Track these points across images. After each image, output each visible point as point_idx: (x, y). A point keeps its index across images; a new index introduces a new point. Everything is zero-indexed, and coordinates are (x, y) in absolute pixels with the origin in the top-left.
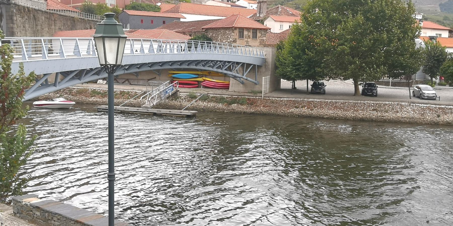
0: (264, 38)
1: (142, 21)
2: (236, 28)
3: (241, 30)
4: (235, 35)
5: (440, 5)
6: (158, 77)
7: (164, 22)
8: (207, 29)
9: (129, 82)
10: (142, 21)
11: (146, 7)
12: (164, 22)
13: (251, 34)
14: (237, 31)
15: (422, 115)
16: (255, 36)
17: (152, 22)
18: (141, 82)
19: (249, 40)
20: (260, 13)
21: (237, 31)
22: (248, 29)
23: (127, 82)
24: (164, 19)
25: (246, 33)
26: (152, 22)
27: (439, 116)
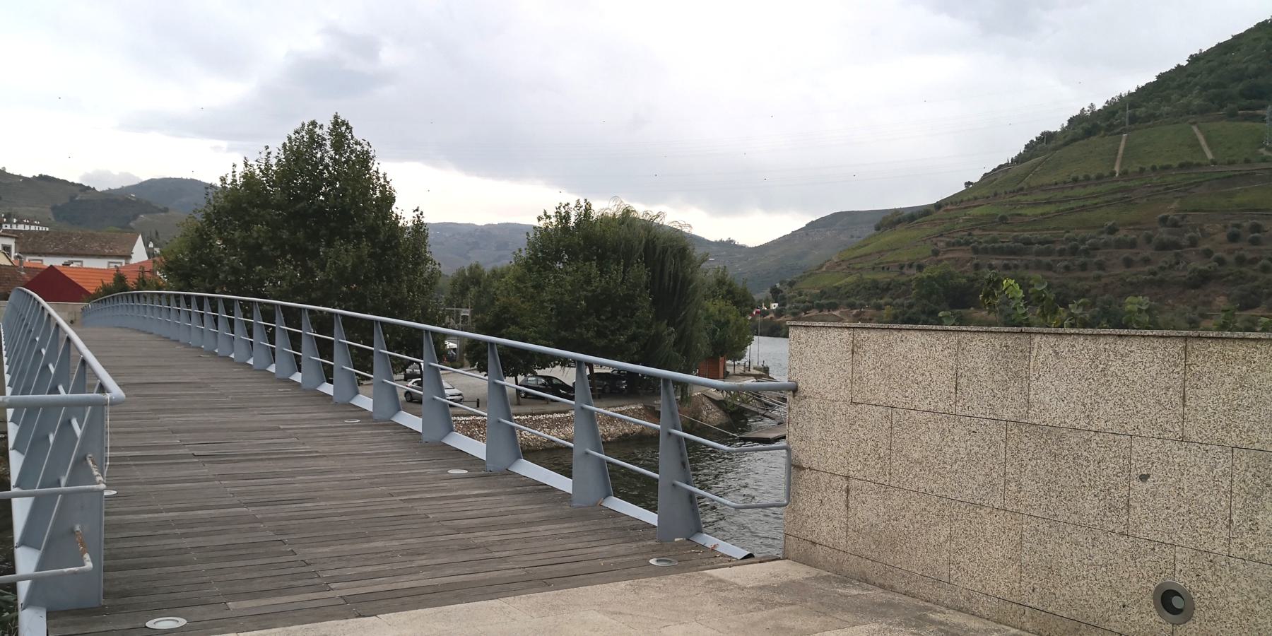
5: (54, 208)
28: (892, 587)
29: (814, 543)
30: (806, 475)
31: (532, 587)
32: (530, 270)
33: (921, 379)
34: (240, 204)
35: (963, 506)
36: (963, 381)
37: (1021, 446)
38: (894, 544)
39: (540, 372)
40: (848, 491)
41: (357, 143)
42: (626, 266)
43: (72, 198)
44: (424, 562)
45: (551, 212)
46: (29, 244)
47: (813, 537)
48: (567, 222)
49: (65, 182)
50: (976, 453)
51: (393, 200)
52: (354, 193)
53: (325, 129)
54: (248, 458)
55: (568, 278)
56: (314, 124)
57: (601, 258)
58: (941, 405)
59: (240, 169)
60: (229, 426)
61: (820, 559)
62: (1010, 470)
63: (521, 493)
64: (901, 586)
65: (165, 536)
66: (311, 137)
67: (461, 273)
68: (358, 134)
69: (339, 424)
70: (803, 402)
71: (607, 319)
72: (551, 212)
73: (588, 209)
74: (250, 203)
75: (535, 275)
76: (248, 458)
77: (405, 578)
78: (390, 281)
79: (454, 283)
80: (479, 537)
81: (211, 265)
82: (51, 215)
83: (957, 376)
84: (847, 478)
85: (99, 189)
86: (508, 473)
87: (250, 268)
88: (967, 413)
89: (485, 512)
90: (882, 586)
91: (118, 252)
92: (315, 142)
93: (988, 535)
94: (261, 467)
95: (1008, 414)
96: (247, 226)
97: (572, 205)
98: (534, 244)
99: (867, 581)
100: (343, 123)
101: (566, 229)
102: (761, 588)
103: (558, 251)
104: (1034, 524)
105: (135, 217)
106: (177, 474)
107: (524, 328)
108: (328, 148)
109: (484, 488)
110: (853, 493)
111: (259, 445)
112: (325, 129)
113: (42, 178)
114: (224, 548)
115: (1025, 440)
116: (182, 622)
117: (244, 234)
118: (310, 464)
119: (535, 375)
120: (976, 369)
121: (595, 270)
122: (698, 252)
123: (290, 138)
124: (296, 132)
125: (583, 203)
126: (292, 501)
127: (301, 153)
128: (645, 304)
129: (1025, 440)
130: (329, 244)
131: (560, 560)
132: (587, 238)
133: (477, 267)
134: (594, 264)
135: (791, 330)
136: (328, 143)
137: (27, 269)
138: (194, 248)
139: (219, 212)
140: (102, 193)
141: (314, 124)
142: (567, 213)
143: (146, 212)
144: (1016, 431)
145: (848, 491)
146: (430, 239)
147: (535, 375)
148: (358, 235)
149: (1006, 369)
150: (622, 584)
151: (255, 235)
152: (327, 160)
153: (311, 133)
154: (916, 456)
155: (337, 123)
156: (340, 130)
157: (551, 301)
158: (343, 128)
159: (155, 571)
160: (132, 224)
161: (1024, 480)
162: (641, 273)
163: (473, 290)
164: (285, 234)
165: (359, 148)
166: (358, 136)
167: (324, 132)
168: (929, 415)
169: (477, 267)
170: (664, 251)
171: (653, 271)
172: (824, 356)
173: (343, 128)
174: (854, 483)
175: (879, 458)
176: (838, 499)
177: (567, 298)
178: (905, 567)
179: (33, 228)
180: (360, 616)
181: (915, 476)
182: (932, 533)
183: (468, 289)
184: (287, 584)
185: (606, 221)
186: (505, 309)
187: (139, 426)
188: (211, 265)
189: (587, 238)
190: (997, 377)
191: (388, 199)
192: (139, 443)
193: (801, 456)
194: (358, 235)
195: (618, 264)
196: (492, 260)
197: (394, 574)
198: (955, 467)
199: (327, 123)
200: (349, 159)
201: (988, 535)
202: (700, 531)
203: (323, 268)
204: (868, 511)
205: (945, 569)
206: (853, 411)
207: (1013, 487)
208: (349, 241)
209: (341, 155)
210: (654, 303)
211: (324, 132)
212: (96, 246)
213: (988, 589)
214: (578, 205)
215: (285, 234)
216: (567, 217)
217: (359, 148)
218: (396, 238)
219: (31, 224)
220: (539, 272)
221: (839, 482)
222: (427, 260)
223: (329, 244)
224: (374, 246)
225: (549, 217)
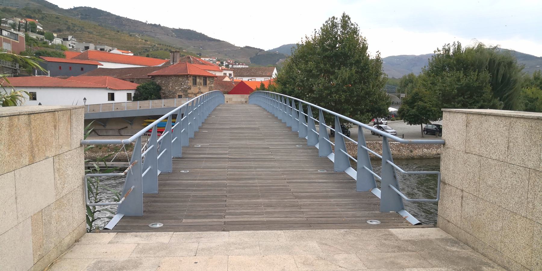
0: (212, 85)
1: (70, 68)
2: (191, 75)
3: (195, 77)
4: (190, 82)
5: (250, 58)
6: (129, 127)
7: (82, 69)
8: (153, 77)
9: (96, 132)
10: (70, 68)
11: (51, 54)
12: (82, 69)
13: (202, 81)
14: (191, 79)
15: (399, 151)
16: (205, 84)
17: (60, 68)
18: (111, 133)
19: (201, 87)
20: (173, 61)
21: (191, 79)
22: (200, 76)
23: (93, 133)
24: (82, 66)
25: (198, 80)
26: (60, 68)
27: (411, 151)
28: (477, 249)
29: (449, 222)
30: (447, 187)
31: (303, 226)
32: (430, 76)
33: (493, 142)
34: (304, 54)
35: (508, 213)
36: (511, 144)
37: (536, 183)
38: (479, 228)
39: (432, 123)
40: (462, 198)
41: (352, 24)
42: (479, 72)
43: (256, 54)
44: (269, 210)
45: (441, 49)
46: (239, 73)
47: (448, 219)
48: (448, 53)
49: (254, 48)
50: (515, 185)
51: (367, 48)
52: (349, 46)
53: (339, 19)
54: (247, 160)
55: (449, 79)
56: (334, 18)
57: (465, 69)
58: (501, 157)
59: (304, 40)
60: (253, 146)
61: (451, 229)
62: (530, 196)
63: (336, 183)
64: (481, 250)
65: (189, 190)
66: (333, 24)
67: (405, 77)
68: (353, 21)
69: (293, 147)
70: (447, 150)
71: (467, 98)
72: (441, 49)
73: (459, 46)
74: (308, 53)
75: (432, 78)
76: (247, 160)
77: (256, 216)
78: (365, 83)
79: (401, 82)
80: (301, 202)
81: (293, 79)
82: (249, 61)
83: (509, 142)
84: (462, 191)
85: (266, 50)
86: (344, 173)
87: (308, 80)
88: (513, 162)
89: (316, 190)
90: (473, 248)
91: (268, 74)
92: (334, 25)
93: (519, 230)
94: (245, 164)
95: (530, 165)
96: (307, 63)
97: (451, 44)
98: (432, 64)
99: (467, 244)
100: (347, 16)
101: (448, 56)
102: (407, 241)
103: (444, 66)
104: (539, 228)
105: (278, 60)
106: (215, 165)
107: (426, 102)
108: (340, 28)
109: (325, 179)
110: (464, 199)
111: (255, 155)
112: (339, 19)
113: (247, 47)
114: (214, 196)
115: (538, 180)
116: (162, 225)
117: (306, 66)
118: (267, 164)
119: (431, 124)
120: (517, 138)
121: (462, 75)
122: (519, 63)
123: (324, 25)
124: (326, 22)
125: (457, 43)
126: (246, 179)
127: (328, 31)
128: (488, 89)
129: (538, 180)
130: (339, 69)
131: (329, 216)
132: (458, 60)
133: (412, 75)
134: (462, 72)
135: (444, 113)
136: (340, 25)
137: (235, 82)
138: (287, 72)
139: (296, 57)
140: (267, 51)
141: (334, 18)
142: (449, 48)
143: (282, 58)
144: (534, 174)
145: (462, 198)
146: (383, 66)
147: (431, 124)
148: (351, 64)
149: (531, 139)
150: (342, 231)
151: (309, 66)
152: (339, 33)
153: (332, 22)
154: (489, 183)
155: (344, 16)
156: (345, 19)
157: (440, 90)
158: (347, 19)
159: (165, 204)
160: (277, 63)
161: (536, 203)
162: (486, 76)
163: (410, 85)
164: (322, 66)
165: (353, 27)
166: (353, 22)
167: (338, 21)
168: (496, 162)
169: (412, 75)
170: (499, 64)
171: (493, 74)
172: (455, 127)
173: (347, 19)
174: (465, 194)
175: (475, 182)
176: (458, 201)
177: (448, 88)
178: (483, 240)
179: (243, 66)
180: (224, 231)
181: (489, 194)
182: (494, 224)
183: (407, 85)
184: (210, 214)
185: (469, 51)
186: (417, 94)
187: (220, 145)
188: (293, 79)
189: (458, 60)
190: (527, 144)
191: (365, 48)
192: (214, 152)
193: (446, 178)
194: (351, 64)
195: (475, 71)
196: (417, 72)
197: (259, 214)
198: (506, 191)
199: (339, 17)
200: (348, 32)
201: (519, 230)
202: (403, 209)
203: (336, 79)
204: (470, 208)
205: (499, 244)
206: (466, 156)
207: (531, 206)
208: (347, 67)
209: (345, 31)
210: (493, 90)
211: (338, 21)
212: (260, 73)
213: (517, 259)
214: (454, 45)
215: (322, 66)
216: (449, 50)
217: (353, 27)
218: (367, 65)
219: (242, 65)
220: (434, 76)
221: (459, 193)
222: (381, 74)
223: (339, 69)
224: (358, 68)
225: (439, 51)
